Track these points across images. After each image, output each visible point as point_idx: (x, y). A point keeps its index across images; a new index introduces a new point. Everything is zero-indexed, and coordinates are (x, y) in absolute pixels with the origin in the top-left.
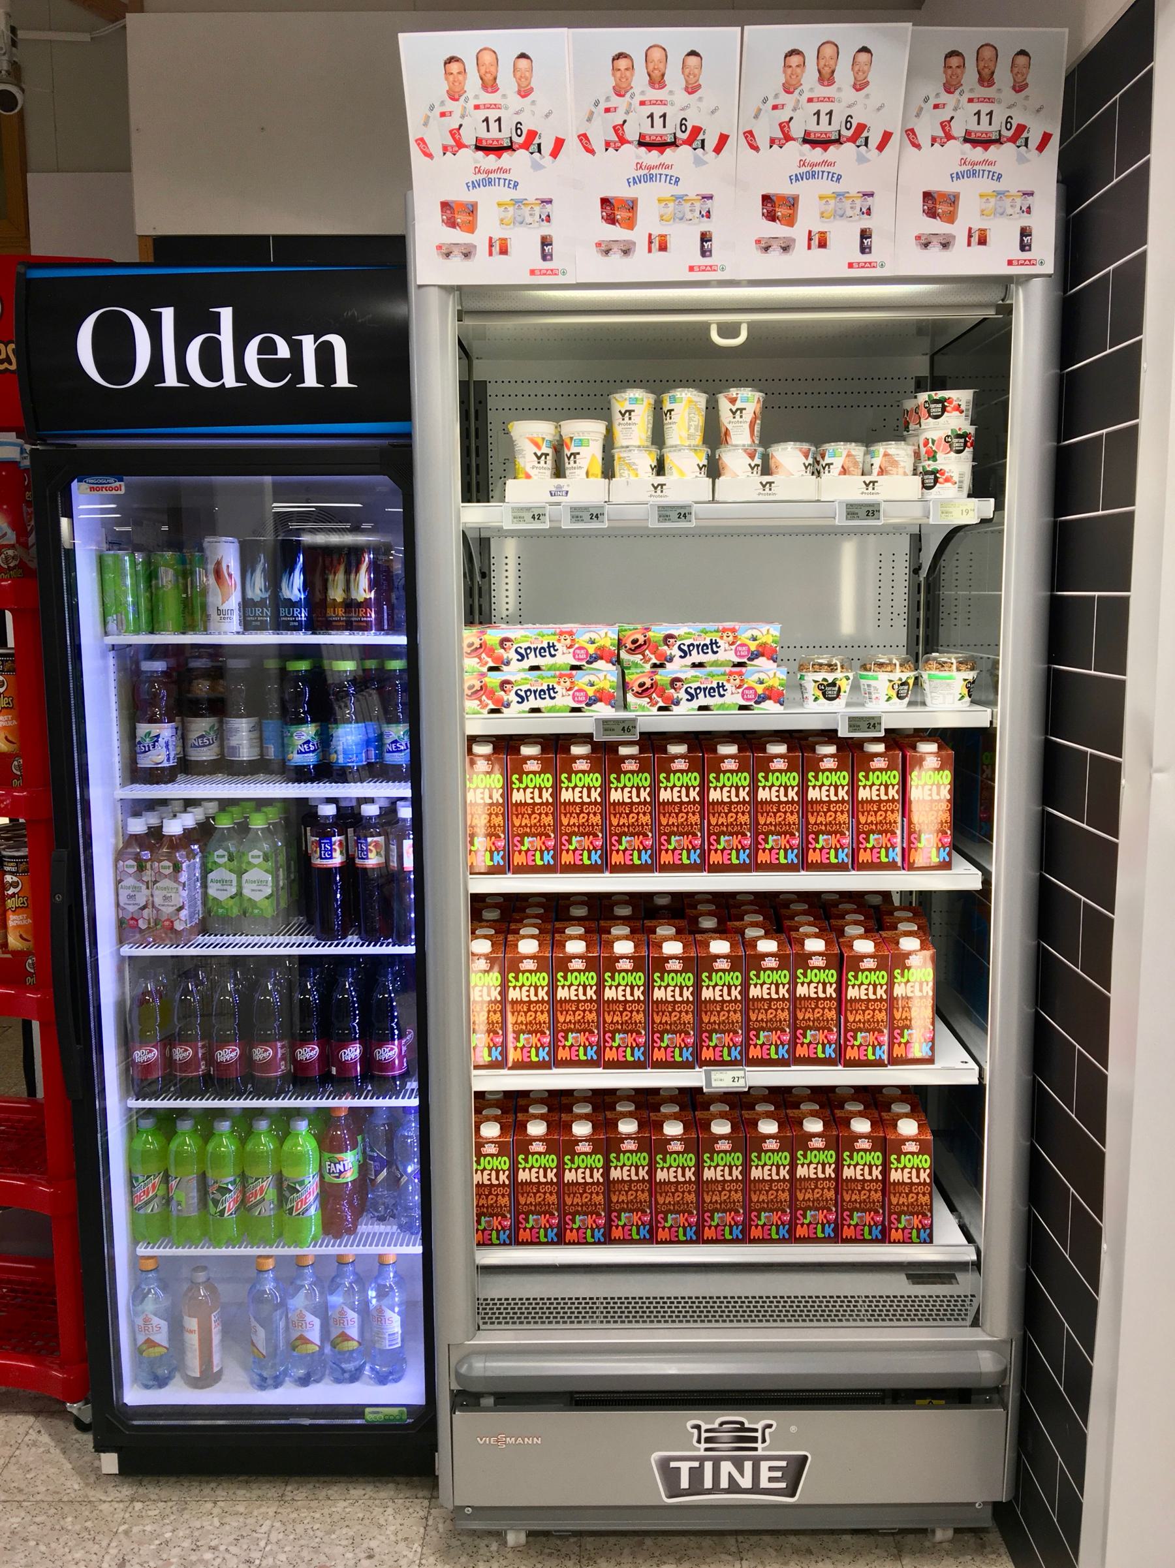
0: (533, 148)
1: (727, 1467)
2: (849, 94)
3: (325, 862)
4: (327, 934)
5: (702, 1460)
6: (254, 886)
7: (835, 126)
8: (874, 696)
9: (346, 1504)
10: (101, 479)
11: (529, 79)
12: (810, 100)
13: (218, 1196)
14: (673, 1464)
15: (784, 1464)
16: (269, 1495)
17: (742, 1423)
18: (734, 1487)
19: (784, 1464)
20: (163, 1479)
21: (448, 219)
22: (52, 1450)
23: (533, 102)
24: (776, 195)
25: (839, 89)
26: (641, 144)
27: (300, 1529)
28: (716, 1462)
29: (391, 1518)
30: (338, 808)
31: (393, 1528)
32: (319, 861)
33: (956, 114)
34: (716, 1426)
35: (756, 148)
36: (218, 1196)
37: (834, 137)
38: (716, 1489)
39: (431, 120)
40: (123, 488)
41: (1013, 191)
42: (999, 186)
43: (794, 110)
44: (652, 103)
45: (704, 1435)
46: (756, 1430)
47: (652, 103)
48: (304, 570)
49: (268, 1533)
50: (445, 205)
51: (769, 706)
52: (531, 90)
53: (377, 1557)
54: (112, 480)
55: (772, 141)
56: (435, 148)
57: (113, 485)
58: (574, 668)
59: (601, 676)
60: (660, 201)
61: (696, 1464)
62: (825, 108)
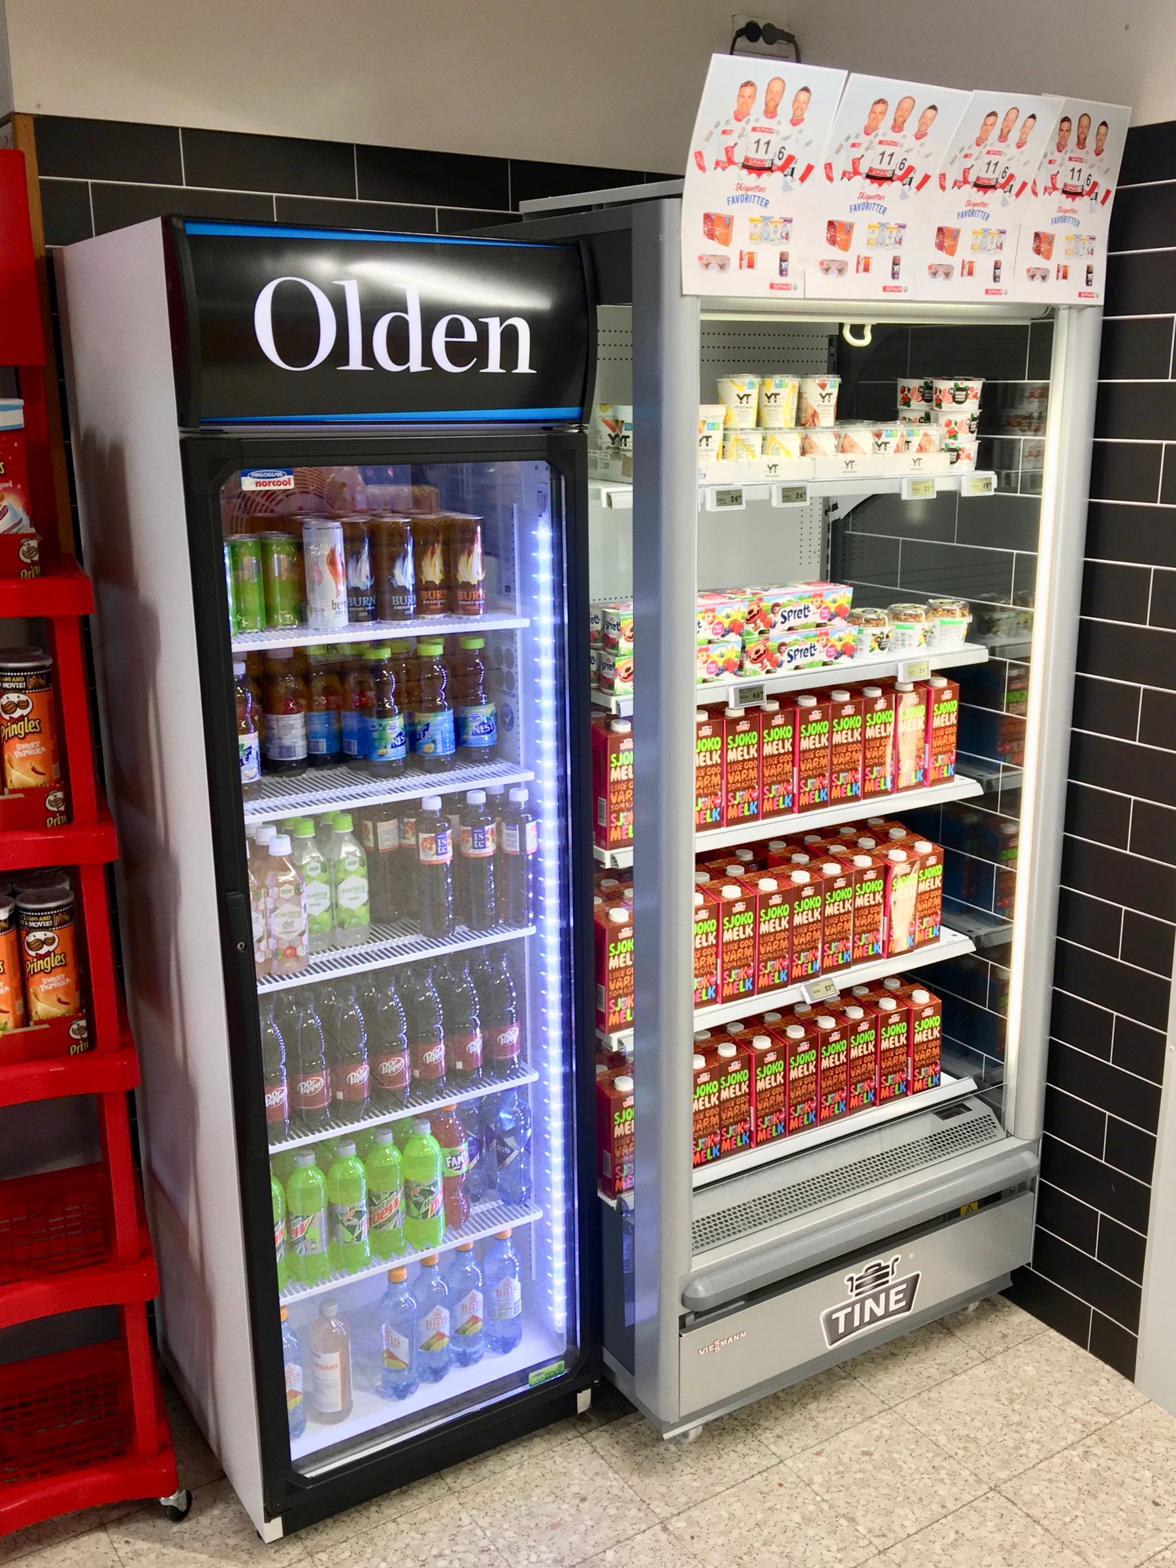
0: (788, 171)
1: (870, 1303)
2: (910, 141)
3: (477, 852)
4: (437, 933)
5: (852, 1305)
6: (351, 895)
7: (770, 156)
8: (907, 643)
9: (514, 1470)
10: (269, 473)
11: (927, 126)
12: (754, 129)
13: (421, 1198)
14: (834, 1316)
15: (904, 1286)
16: (437, 1494)
17: (879, 1265)
18: (874, 1318)
19: (904, 1286)
20: (342, 1517)
21: (709, 230)
22: (165, 1551)
23: (800, 132)
24: (716, 215)
25: (779, 122)
26: (745, 166)
27: (498, 1506)
28: (862, 1302)
29: (565, 1464)
30: (487, 795)
31: (576, 1470)
32: (471, 851)
33: (866, 154)
34: (863, 1273)
35: (830, 178)
36: (421, 1198)
37: (768, 165)
38: (863, 1324)
39: (713, 136)
40: (292, 482)
41: (777, 218)
42: (766, 212)
43: (740, 136)
44: (763, 130)
45: (855, 1283)
46: (887, 1267)
47: (763, 130)
48: (87, 578)
49: (473, 1521)
50: (707, 217)
51: (845, 660)
52: (802, 120)
53: (589, 1497)
54: (279, 473)
55: (717, 163)
56: (709, 163)
57: (281, 479)
58: (710, 642)
59: (730, 646)
60: (751, 220)
61: (849, 1310)
62: (765, 137)
